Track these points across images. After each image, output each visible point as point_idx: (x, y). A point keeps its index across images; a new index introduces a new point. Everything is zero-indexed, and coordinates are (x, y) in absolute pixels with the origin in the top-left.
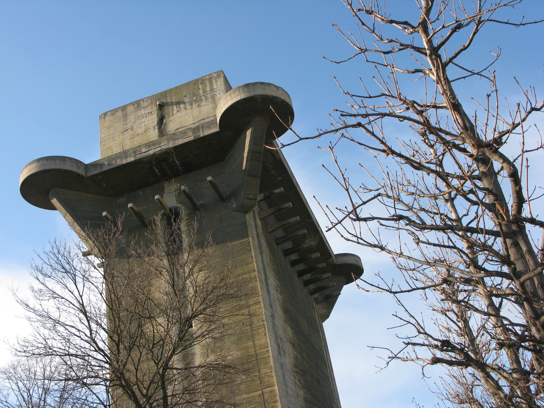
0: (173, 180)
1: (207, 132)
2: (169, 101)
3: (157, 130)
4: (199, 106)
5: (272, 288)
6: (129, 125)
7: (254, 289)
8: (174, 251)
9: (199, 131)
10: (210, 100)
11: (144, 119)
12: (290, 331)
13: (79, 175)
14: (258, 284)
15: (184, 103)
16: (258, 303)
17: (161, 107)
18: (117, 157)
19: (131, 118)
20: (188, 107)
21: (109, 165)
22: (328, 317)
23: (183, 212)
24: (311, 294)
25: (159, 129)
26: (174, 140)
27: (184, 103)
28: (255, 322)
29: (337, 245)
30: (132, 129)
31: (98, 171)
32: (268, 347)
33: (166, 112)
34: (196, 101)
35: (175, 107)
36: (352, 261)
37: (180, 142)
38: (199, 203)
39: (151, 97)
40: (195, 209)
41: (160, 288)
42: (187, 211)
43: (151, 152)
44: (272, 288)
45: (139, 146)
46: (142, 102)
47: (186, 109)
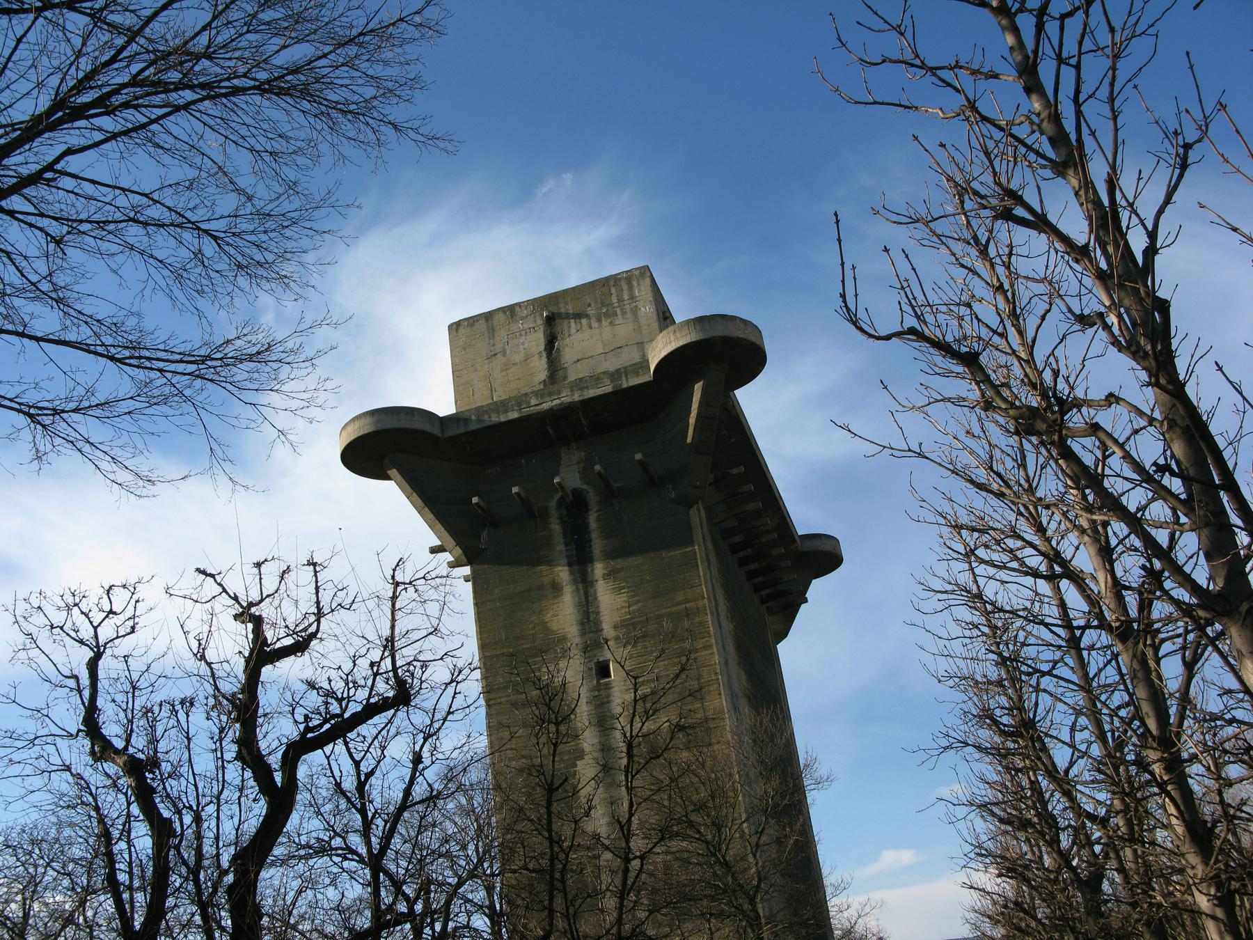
0: (574, 445)
2: (563, 310)
4: (611, 324)
5: (723, 618)
6: (499, 347)
7: (703, 624)
8: (580, 560)
9: (620, 377)
10: (629, 315)
12: (744, 677)
13: (432, 436)
15: (587, 316)
16: (707, 647)
17: (550, 320)
18: (492, 410)
19: (501, 334)
20: (595, 324)
21: (479, 421)
23: (593, 499)
24: (763, 602)
25: (548, 358)
26: (582, 389)
27: (587, 316)
28: (704, 674)
29: (806, 517)
30: (504, 353)
31: (462, 430)
33: (559, 329)
34: (607, 315)
35: (572, 321)
36: (827, 547)
37: (591, 393)
40: (610, 494)
41: (563, 615)
43: (546, 406)
45: (526, 394)
46: (517, 309)
47: (591, 327)
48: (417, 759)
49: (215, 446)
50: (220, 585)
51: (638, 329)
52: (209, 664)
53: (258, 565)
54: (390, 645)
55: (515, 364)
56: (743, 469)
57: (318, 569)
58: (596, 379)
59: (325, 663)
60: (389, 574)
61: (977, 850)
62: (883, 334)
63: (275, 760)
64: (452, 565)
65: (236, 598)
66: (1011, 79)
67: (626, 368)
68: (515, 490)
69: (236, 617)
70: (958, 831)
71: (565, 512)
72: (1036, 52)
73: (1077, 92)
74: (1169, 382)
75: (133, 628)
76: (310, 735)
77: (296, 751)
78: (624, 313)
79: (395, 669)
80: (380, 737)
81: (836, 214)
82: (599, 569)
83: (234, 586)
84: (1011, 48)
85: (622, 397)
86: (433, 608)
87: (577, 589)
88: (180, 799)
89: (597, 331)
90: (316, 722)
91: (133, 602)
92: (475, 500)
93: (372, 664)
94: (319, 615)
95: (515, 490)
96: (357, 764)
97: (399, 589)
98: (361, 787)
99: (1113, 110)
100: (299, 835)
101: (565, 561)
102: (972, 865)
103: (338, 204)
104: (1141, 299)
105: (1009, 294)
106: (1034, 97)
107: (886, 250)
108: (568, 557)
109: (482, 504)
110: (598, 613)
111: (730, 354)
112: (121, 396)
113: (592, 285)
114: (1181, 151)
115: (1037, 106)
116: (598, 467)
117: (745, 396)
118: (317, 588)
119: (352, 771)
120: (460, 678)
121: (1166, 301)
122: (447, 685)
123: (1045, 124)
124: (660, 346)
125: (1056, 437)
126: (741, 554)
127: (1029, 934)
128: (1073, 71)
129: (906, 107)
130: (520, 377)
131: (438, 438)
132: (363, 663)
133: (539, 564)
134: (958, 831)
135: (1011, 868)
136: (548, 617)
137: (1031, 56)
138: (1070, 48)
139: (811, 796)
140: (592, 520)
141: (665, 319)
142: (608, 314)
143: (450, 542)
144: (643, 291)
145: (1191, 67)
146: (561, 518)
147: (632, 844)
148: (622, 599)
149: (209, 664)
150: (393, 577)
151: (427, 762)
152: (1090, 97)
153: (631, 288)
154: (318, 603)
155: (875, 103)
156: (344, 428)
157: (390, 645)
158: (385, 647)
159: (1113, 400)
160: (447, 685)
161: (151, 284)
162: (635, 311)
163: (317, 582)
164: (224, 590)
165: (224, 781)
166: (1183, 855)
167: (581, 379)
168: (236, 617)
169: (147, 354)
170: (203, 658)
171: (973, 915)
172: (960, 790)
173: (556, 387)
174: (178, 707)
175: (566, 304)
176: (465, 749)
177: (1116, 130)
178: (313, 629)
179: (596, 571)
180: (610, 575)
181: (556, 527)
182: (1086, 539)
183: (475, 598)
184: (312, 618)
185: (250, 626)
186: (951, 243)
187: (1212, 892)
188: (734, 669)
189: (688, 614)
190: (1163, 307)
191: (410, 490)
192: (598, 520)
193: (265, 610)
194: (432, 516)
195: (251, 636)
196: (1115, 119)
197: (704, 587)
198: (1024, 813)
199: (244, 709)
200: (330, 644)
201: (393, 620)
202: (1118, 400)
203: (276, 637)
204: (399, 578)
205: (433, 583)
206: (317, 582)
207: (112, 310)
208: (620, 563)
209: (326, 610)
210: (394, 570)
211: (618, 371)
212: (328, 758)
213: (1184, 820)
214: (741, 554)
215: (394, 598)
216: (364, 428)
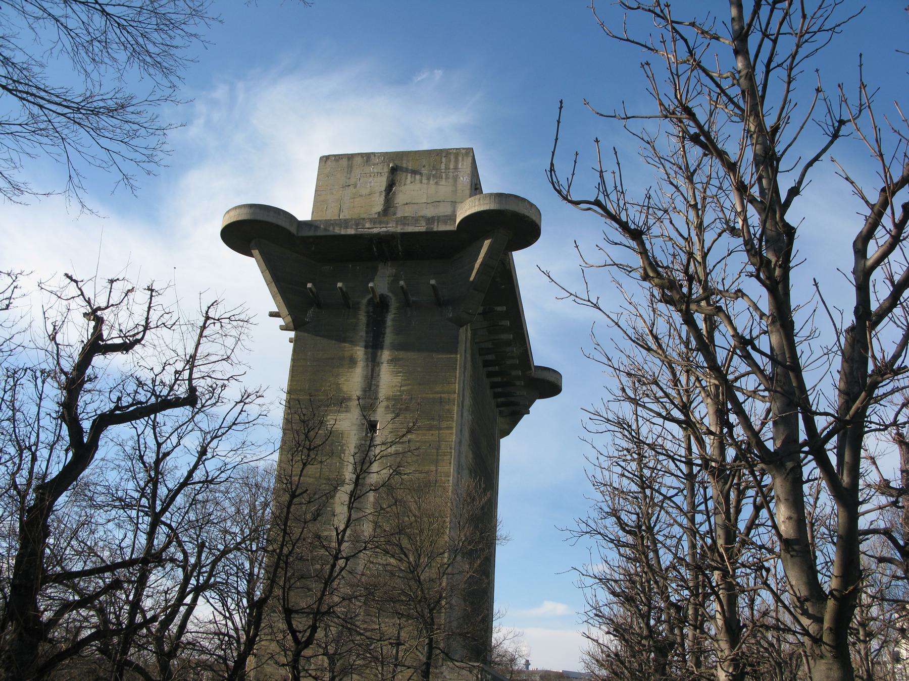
1: (443, 228)
2: (404, 166)
3: (383, 197)
4: (436, 183)
5: (466, 408)
6: (353, 181)
7: (450, 411)
8: (374, 346)
9: (433, 223)
11: (371, 179)
12: (471, 455)
13: (289, 233)
14: (456, 408)
15: (421, 174)
17: (394, 170)
18: (337, 224)
19: (357, 172)
20: (425, 181)
21: (325, 230)
24: (498, 406)
26: (404, 224)
27: (421, 174)
29: (543, 354)
30: (355, 187)
31: (311, 233)
32: (449, 476)
36: (552, 378)
37: (410, 229)
38: (412, 299)
40: (406, 304)
41: (353, 382)
43: (375, 231)
44: (466, 408)
46: (372, 157)
48: (203, 452)
49: (73, 174)
50: (80, 289)
51: (455, 192)
52: (57, 345)
53: (112, 281)
54: (191, 361)
55: (361, 196)
56: (505, 308)
57: (154, 294)
58: (416, 220)
59: (142, 363)
60: (204, 309)
61: (594, 611)
62: (574, 199)
63: (86, 425)
64: (283, 328)
65: (89, 302)
66: (727, 42)
67: (439, 217)
68: (340, 285)
69: (85, 315)
70: (585, 595)
71: (371, 309)
72: (750, 25)
73: (770, 60)
74: (768, 278)
75: (8, 306)
76: (118, 412)
77: (103, 421)
78: (447, 178)
79: (190, 379)
80: (179, 430)
81: (561, 102)
82: (386, 355)
83: (88, 294)
84: (733, 19)
85: (430, 237)
86: (230, 342)
87: (367, 366)
88: (24, 441)
89: (425, 186)
90: (125, 404)
91: (12, 287)
92: (309, 285)
93: (176, 372)
94: (146, 327)
95: (340, 285)
96: (159, 445)
97: (209, 322)
98: (158, 461)
99: (789, 76)
100: (117, 490)
101: (363, 344)
102: (591, 621)
103: (206, 15)
104: (777, 223)
105: (700, 212)
106: (740, 58)
107: (597, 141)
108: (366, 341)
109: (314, 289)
110: (378, 386)
111: (515, 225)
112: (12, 121)
113: (429, 153)
114: (836, 124)
115: (740, 65)
116: (402, 283)
117: (520, 258)
118: (149, 308)
119: (155, 448)
120: (247, 401)
121: (793, 228)
122: (237, 403)
123: (742, 80)
124: (467, 207)
125: (684, 307)
126: (490, 369)
127: (621, 678)
128: (771, 43)
129: (649, 49)
130: (362, 208)
131: (293, 235)
132: (170, 370)
133: (344, 341)
134: (585, 595)
135: (619, 630)
136: (342, 380)
137: (746, 27)
138: (773, 29)
139: (499, 549)
140: (390, 319)
141: (476, 189)
142: (436, 175)
143: (285, 311)
144: (465, 166)
145: (861, 66)
146: (368, 312)
147: (342, 548)
148: (398, 380)
149: (57, 345)
150: (207, 312)
151: (209, 455)
152: (778, 66)
153: (457, 161)
154: (147, 319)
155: (628, 40)
156: (228, 212)
157: (191, 361)
158: (188, 362)
159: (740, 294)
160: (237, 403)
161: (60, 45)
162: (456, 178)
163: (150, 303)
164: (82, 294)
165: (59, 435)
166: (717, 641)
167: (405, 217)
168: (85, 315)
169: (35, 91)
170: (54, 339)
171: (588, 657)
172: (600, 568)
173: (385, 219)
174: (38, 374)
175: (408, 161)
176: (239, 452)
177: (788, 91)
178: (139, 337)
179: (384, 356)
180: (393, 361)
181: (363, 318)
182: (709, 400)
183: (293, 355)
184: (141, 328)
185: (92, 324)
186: (667, 165)
187: (730, 671)
188: (465, 448)
189: (441, 401)
190: (790, 231)
191: (265, 268)
192: (393, 320)
193: (106, 315)
194: (276, 289)
195: (91, 331)
196: (789, 83)
197: (457, 384)
198: (637, 590)
199: (75, 382)
200: (149, 350)
201: (198, 344)
202: (743, 295)
203: (111, 335)
204: (211, 314)
205: (235, 323)
206: (150, 303)
207: (24, 58)
208: (402, 354)
209: (152, 325)
210: (209, 308)
211: (433, 218)
212: (139, 436)
213: (724, 616)
214: (490, 369)
215: (204, 327)
216: (242, 216)
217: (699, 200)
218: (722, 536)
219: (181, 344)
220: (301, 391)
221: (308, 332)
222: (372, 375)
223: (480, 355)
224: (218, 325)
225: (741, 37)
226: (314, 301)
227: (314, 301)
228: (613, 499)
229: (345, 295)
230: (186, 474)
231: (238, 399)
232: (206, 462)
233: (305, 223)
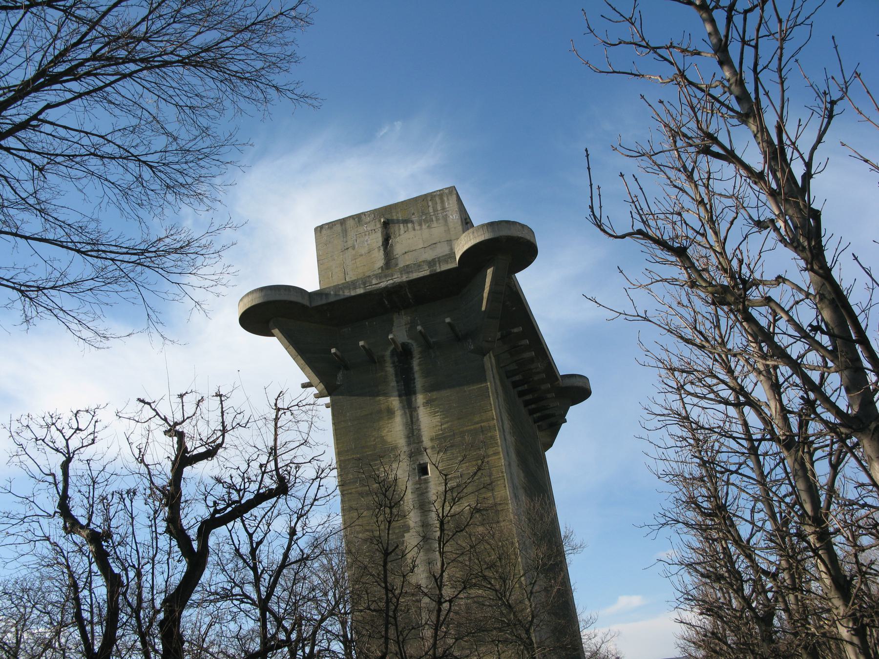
2: (395, 218)
3: (382, 252)
6: (350, 243)
7: (493, 438)
8: (407, 392)
9: (435, 264)
10: (441, 221)
11: (367, 238)
12: (522, 475)
13: (303, 306)
15: (412, 222)
17: (386, 225)
18: (345, 287)
19: (352, 234)
20: (417, 227)
21: (336, 295)
22: (551, 445)
24: (535, 422)
25: (385, 251)
26: (408, 273)
27: (412, 222)
28: (494, 473)
29: (565, 362)
30: (354, 248)
31: (324, 302)
34: (426, 221)
35: (401, 225)
37: (415, 275)
38: (432, 340)
39: (374, 212)
40: (427, 346)
41: (395, 431)
42: (420, 349)
43: (383, 285)
44: (507, 430)
46: (363, 216)
47: (414, 230)
48: (293, 532)
49: (151, 313)
50: (154, 410)
51: (448, 231)
52: (147, 466)
54: (273, 452)
55: (361, 255)
57: (223, 399)
58: (418, 266)
59: (228, 465)
60: (273, 402)
61: (686, 596)
63: (193, 533)
64: (317, 396)
65: (165, 420)
66: (709, 55)
67: (439, 258)
68: (361, 343)
69: (166, 433)
70: (672, 582)
71: (396, 359)
72: (727, 36)
73: (756, 65)
74: (820, 268)
75: (93, 440)
76: (217, 515)
77: (207, 526)
78: (437, 220)
79: (277, 469)
80: (266, 517)
81: (586, 150)
82: (420, 399)
84: (710, 34)
86: (304, 426)
89: (419, 232)
90: (222, 506)
91: (93, 422)
92: (333, 350)
94: (224, 431)
95: (361, 343)
96: (250, 536)
97: (280, 413)
98: (253, 551)
99: (780, 77)
101: (396, 393)
103: (237, 143)
104: (801, 210)
105: (708, 206)
106: (726, 68)
107: (622, 175)
108: (398, 390)
109: (338, 353)
110: (419, 430)
111: (512, 249)
112: (85, 277)
113: (415, 199)
114: (828, 106)
115: (728, 74)
116: (419, 328)
117: (523, 278)
118: (222, 412)
119: (247, 541)
120: (322, 476)
121: (818, 211)
122: (314, 480)
123: (733, 87)
124: (463, 242)
125: (741, 307)
126: (520, 389)
127: (722, 655)
128: (753, 50)
129: (636, 75)
130: (365, 265)
131: (307, 307)
132: (255, 465)
133: (378, 395)
134: (672, 582)
135: (709, 609)
136: (384, 433)
138: (751, 34)
139: (569, 558)
140: (416, 364)
141: (467, 223)
142: (426, 220)
143: (316, 380)
144: (451, 204)
145: (836, 47)
146: (393, 363)
147: (443, 592)
148: (437, 419)
149: (147, 466)
150: (276, 405)
152: (765, 68)
153: (442, 202)
154: (223, 422)
155: (614, 72)
156: (241, 300)
157: (273, 452)
158: (270, 454)
159: (781, 280)
160: (314, 480)
161: (106, 199)
162: (445, 218)
163: (222, 408)
164: (157, 414)
165: (157, 547)
168: (166, 433)
170: (142, 461)
171: (682, 641)
173: (390, 271)
174: (125, 496)
175: (397, 213)
176: (326, 525)
177: (783, 91)
178: (219, 441)
179: (418, 401)
180: (428, 403)
181: (390, 369)
182: (762, 378)
183: (333, 419)
184: (219, 433)
185: (176, 439)
186: (667, 170)
187: (851, 625)
188: (515, 469)
189: (482, 430)
192: (419, 365)
193: (186, 428)
194: (303, 362)
195: (176, 446)
196: (782, 83)
197: (493, 410)
198: (718, 569)
199: (171, 497)
201: (276, 435)
202: (784, 280)
203: (194, 446)
204: (280, 405)
205: (304, 408)
206: (222, 408)
207: (78, 217)
208: (435, 395)
209: (229, 428)
210: (276, 400)
211: (433, 260)
212: (230, 531)
213: (831, 575)
214: (520, 389)
215: (276, 419)
216: (256, 300)
217: (704, 196)
218: (808, 500)
219: (260, 438)
220: (348, 451)
221: (342, 394)
222: (412, 421)
223: (508, 377)
224: (288, 413)
225: (721, 50)
226: (341, 364)
227: (341, 364)
228: (688, 490)
229: (368, 352)
230: (281, 557)
231: (314, 475)
232: (299, 542)
233: (315, 293)
